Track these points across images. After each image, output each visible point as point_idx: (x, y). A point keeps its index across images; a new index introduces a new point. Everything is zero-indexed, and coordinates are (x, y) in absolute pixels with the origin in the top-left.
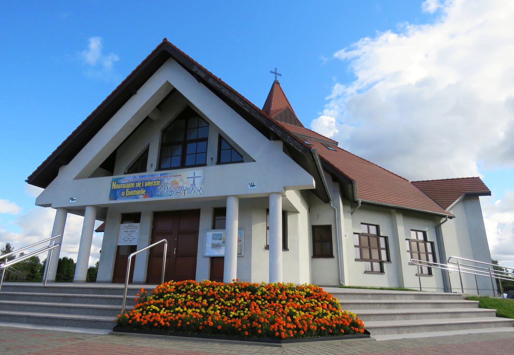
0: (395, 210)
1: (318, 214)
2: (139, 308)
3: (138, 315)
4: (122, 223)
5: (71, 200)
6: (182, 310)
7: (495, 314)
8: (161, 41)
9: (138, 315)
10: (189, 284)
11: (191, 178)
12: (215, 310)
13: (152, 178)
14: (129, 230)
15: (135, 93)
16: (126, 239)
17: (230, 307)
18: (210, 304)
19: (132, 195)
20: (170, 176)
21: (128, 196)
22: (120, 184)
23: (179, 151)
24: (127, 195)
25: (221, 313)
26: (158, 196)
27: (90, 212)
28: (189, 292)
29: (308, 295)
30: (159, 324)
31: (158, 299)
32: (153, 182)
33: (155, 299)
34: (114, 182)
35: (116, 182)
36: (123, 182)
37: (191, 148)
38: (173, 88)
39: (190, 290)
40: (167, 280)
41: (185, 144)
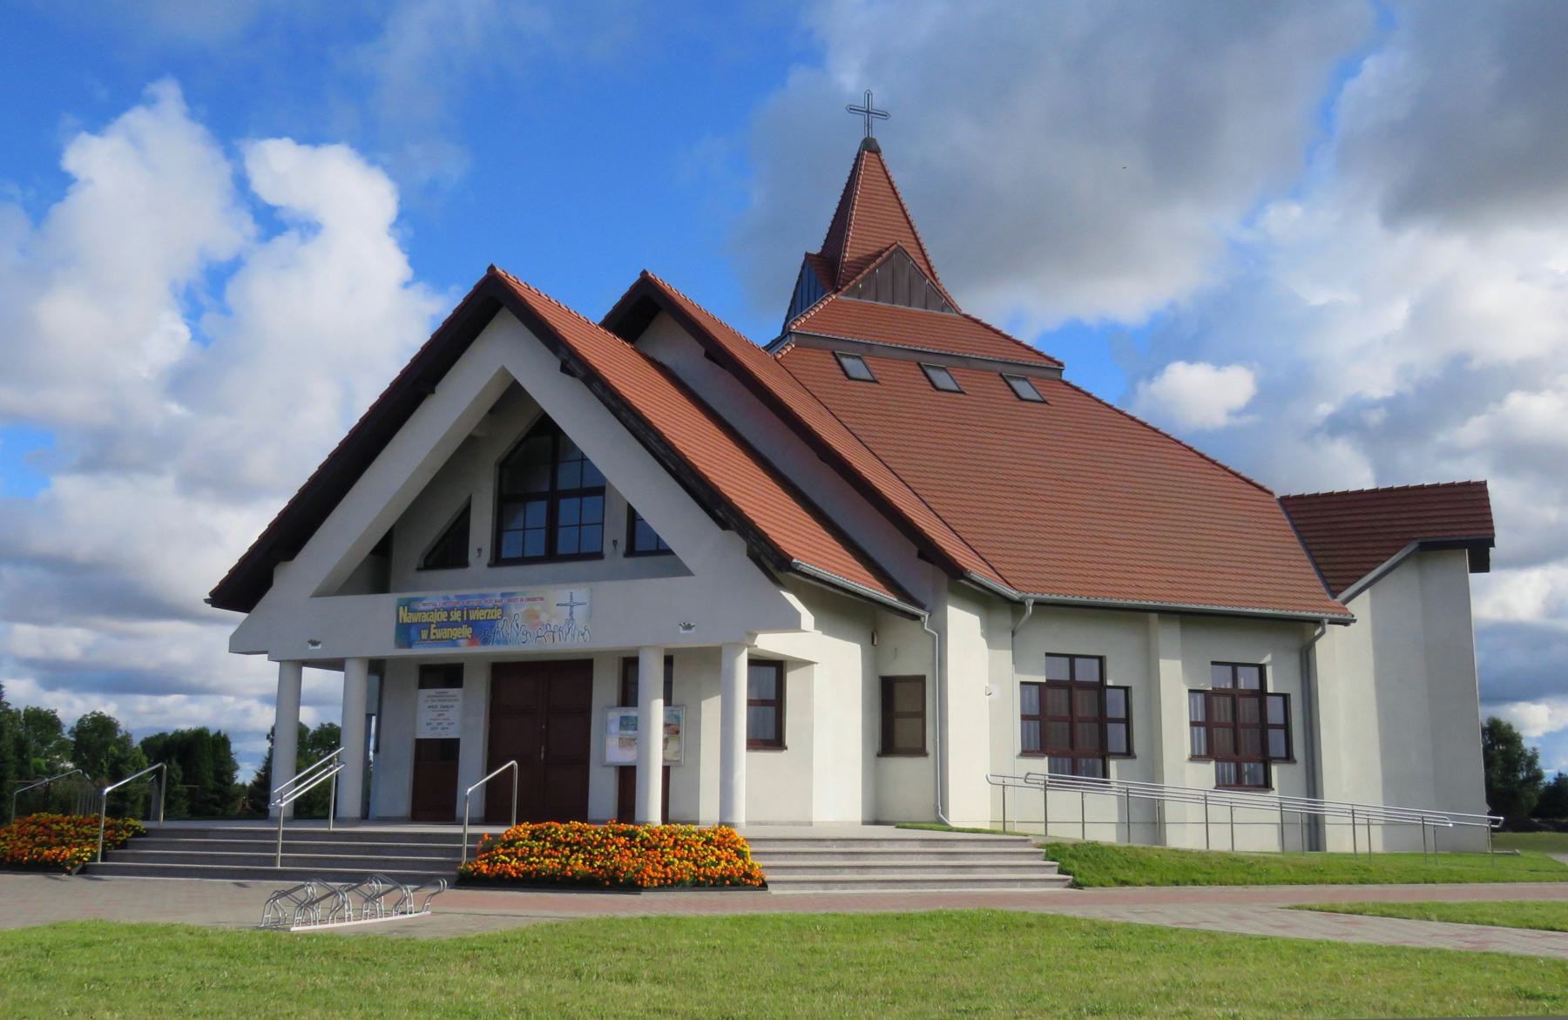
0: (1156, 615)
1: (896, 649)
2: (484, 859)
3: (484, 867)
4: (422, 686)
5: (310, 645)
6: (537, 860)
7: (1056, 869)
8: (483, 273)
9: (484, 867)
10: (549, 828)
11: (566, 605)
12: (577, 859)
13: (483, 602)
14: (439, 704)
15: (433, 391)
16: (435, 724)
17: (597, 856)
18: (572, 852)
19: (444, 637)
20: (522, 600)
21: (436, 639)
22: (415, 611)
23: (537, 512)
24: (432, 637)
25: (584, 863)
26: (498, 642)
27: (358, 672)
28: (549, 839)
29: (708, 842)
30: (511, 876)
31: (508, 848)
32: (486, 611)
33: (503, 847)
34: (401, 608)
35: (406, 608)
36: (421, 607)
37: (568, 509)
38: (512, 380)
39: (549, 835)
40: (519, 822)
41: (553, 498)
